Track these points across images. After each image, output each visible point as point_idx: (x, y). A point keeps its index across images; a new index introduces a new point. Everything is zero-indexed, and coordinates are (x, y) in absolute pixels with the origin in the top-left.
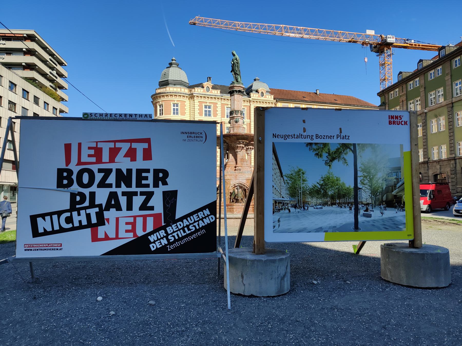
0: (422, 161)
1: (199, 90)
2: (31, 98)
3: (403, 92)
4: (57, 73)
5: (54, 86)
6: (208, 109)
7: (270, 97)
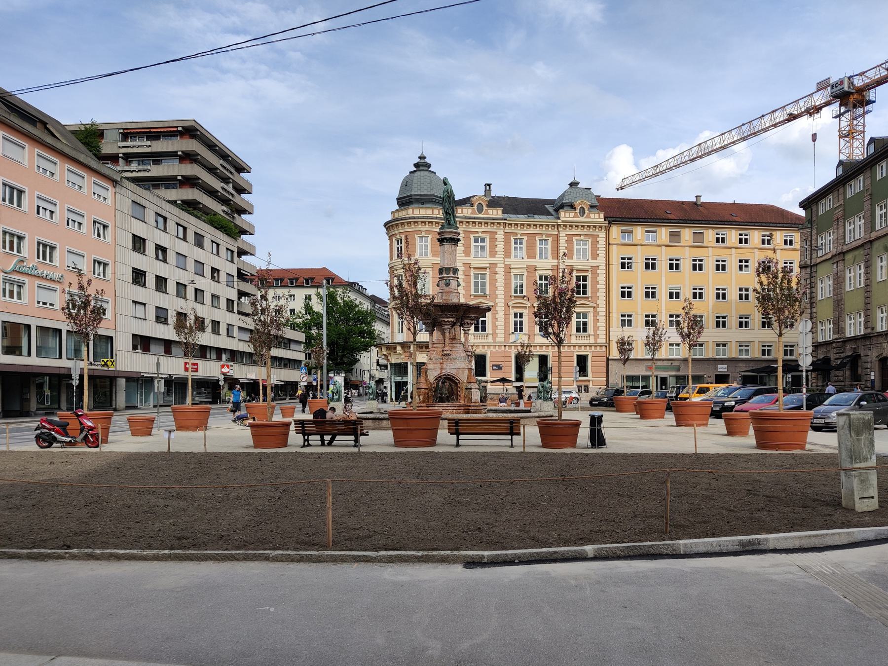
0: (862, 333)
1: (465, 211)
3: (838, 201)
4: (234, 188)
5: (229, 212)
6: (480, 244)
7: (597, 216)
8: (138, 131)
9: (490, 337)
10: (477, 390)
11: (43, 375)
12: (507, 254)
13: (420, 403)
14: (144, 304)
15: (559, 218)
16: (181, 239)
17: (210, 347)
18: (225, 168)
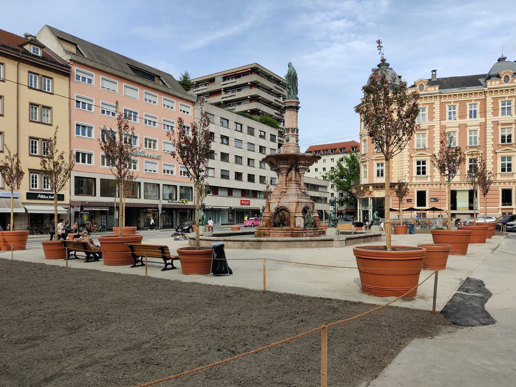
1: (493, 83)
2: (245, 129)
5: (279, 113)
8: (230, 74)
9: (429, 178)
10: (302, 218)
11: (188, 209)
12: (442, 118)
13: (263, 227)
14: (214, 169)
15: (486, 87)
16: (239, 131)
17: (260, 192)
18: (277, 88)
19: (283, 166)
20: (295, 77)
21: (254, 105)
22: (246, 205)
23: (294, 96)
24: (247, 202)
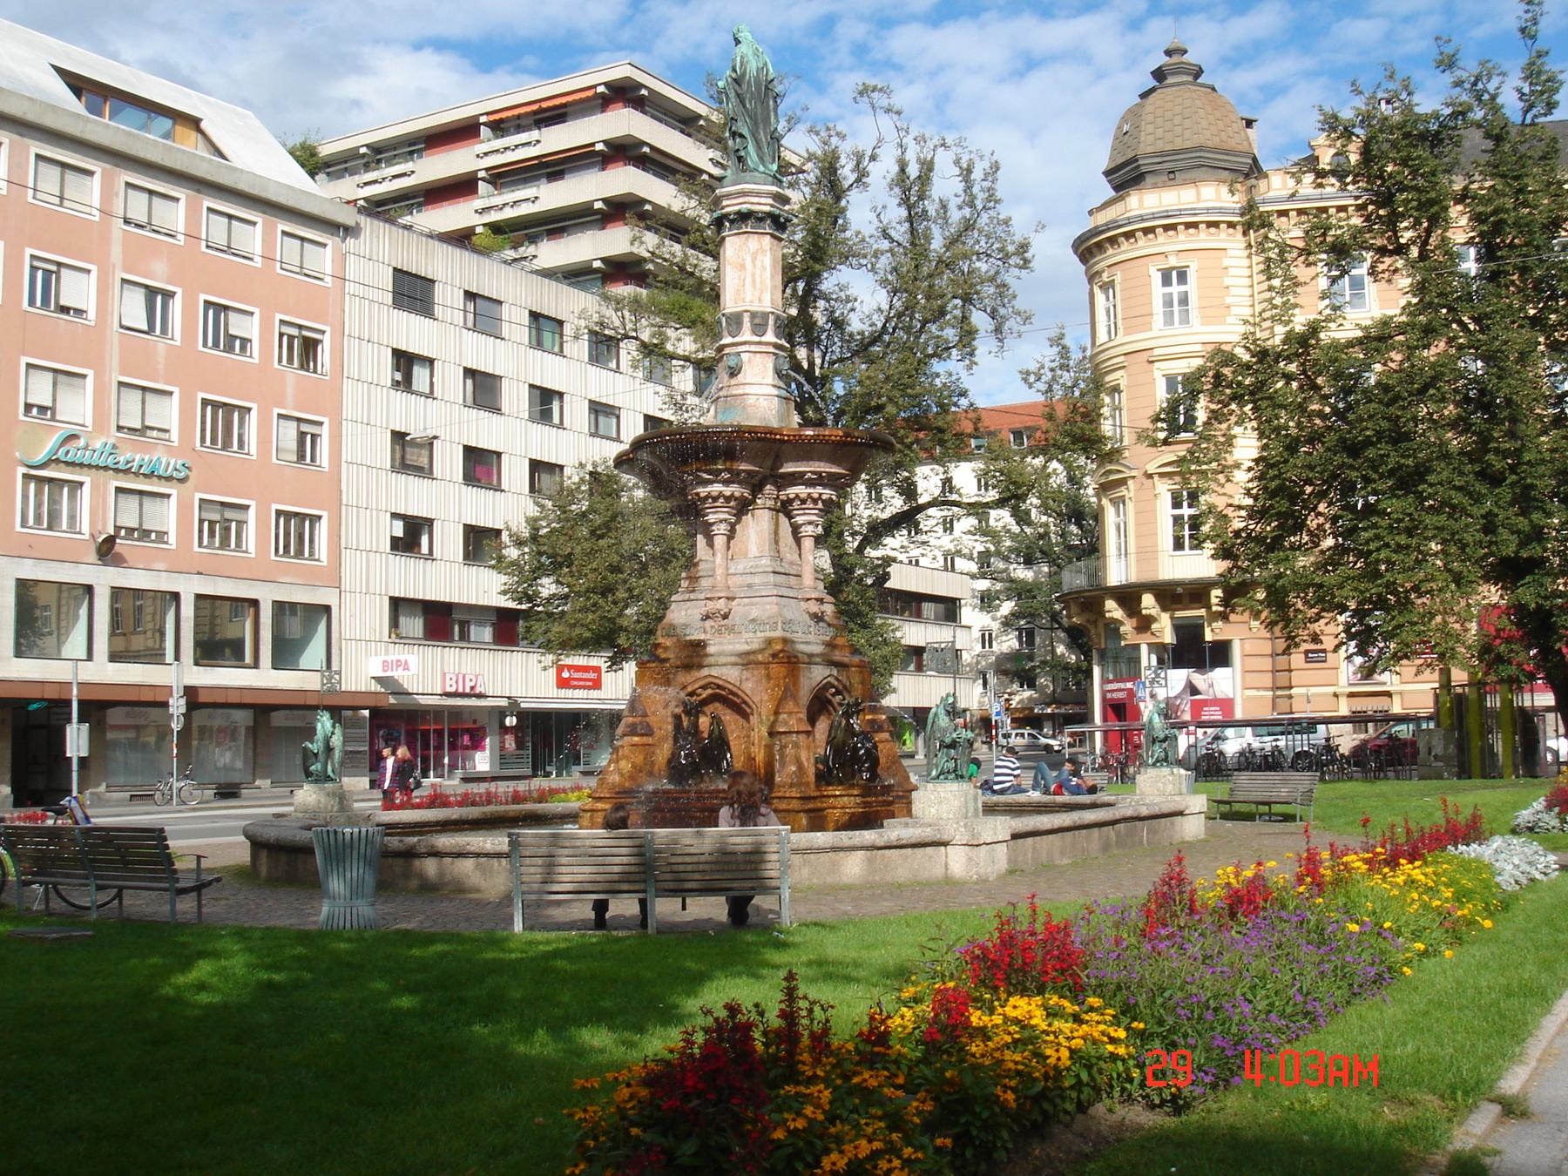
19: (716, 488)
20: (767, 88)
21: (616, 241)
22: (585, 687)
23: (761, 168)
24: (586, 675)
